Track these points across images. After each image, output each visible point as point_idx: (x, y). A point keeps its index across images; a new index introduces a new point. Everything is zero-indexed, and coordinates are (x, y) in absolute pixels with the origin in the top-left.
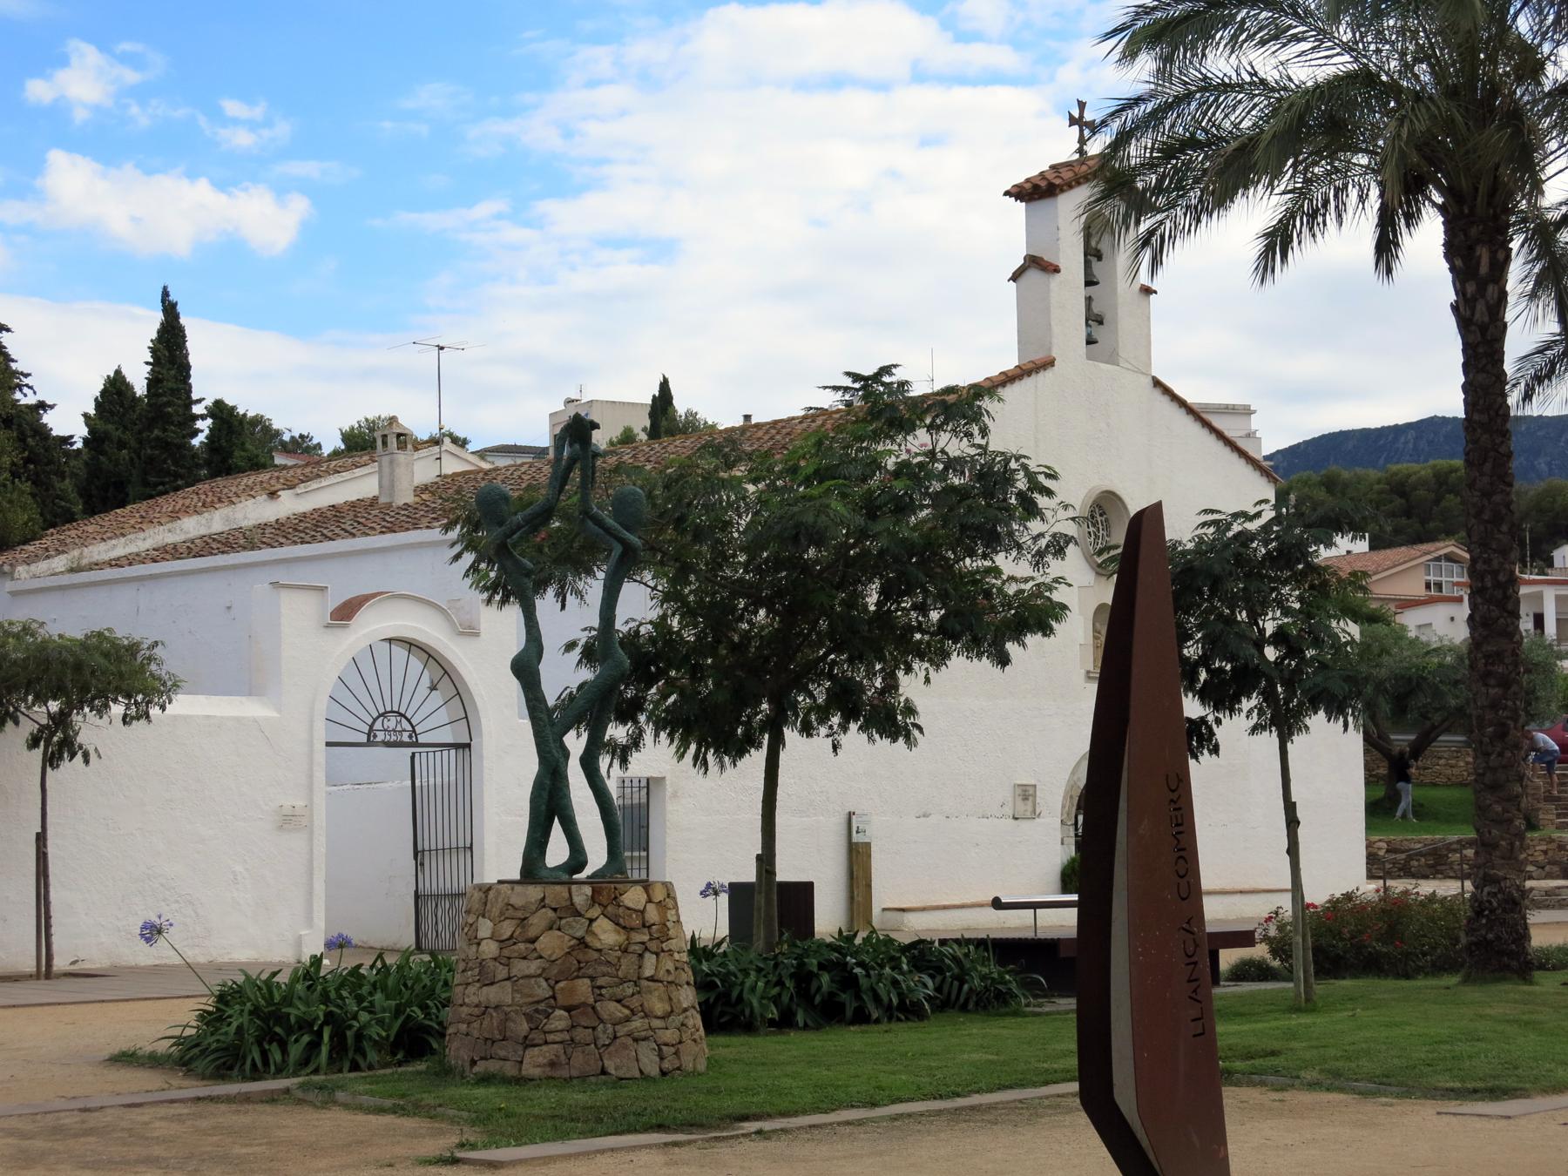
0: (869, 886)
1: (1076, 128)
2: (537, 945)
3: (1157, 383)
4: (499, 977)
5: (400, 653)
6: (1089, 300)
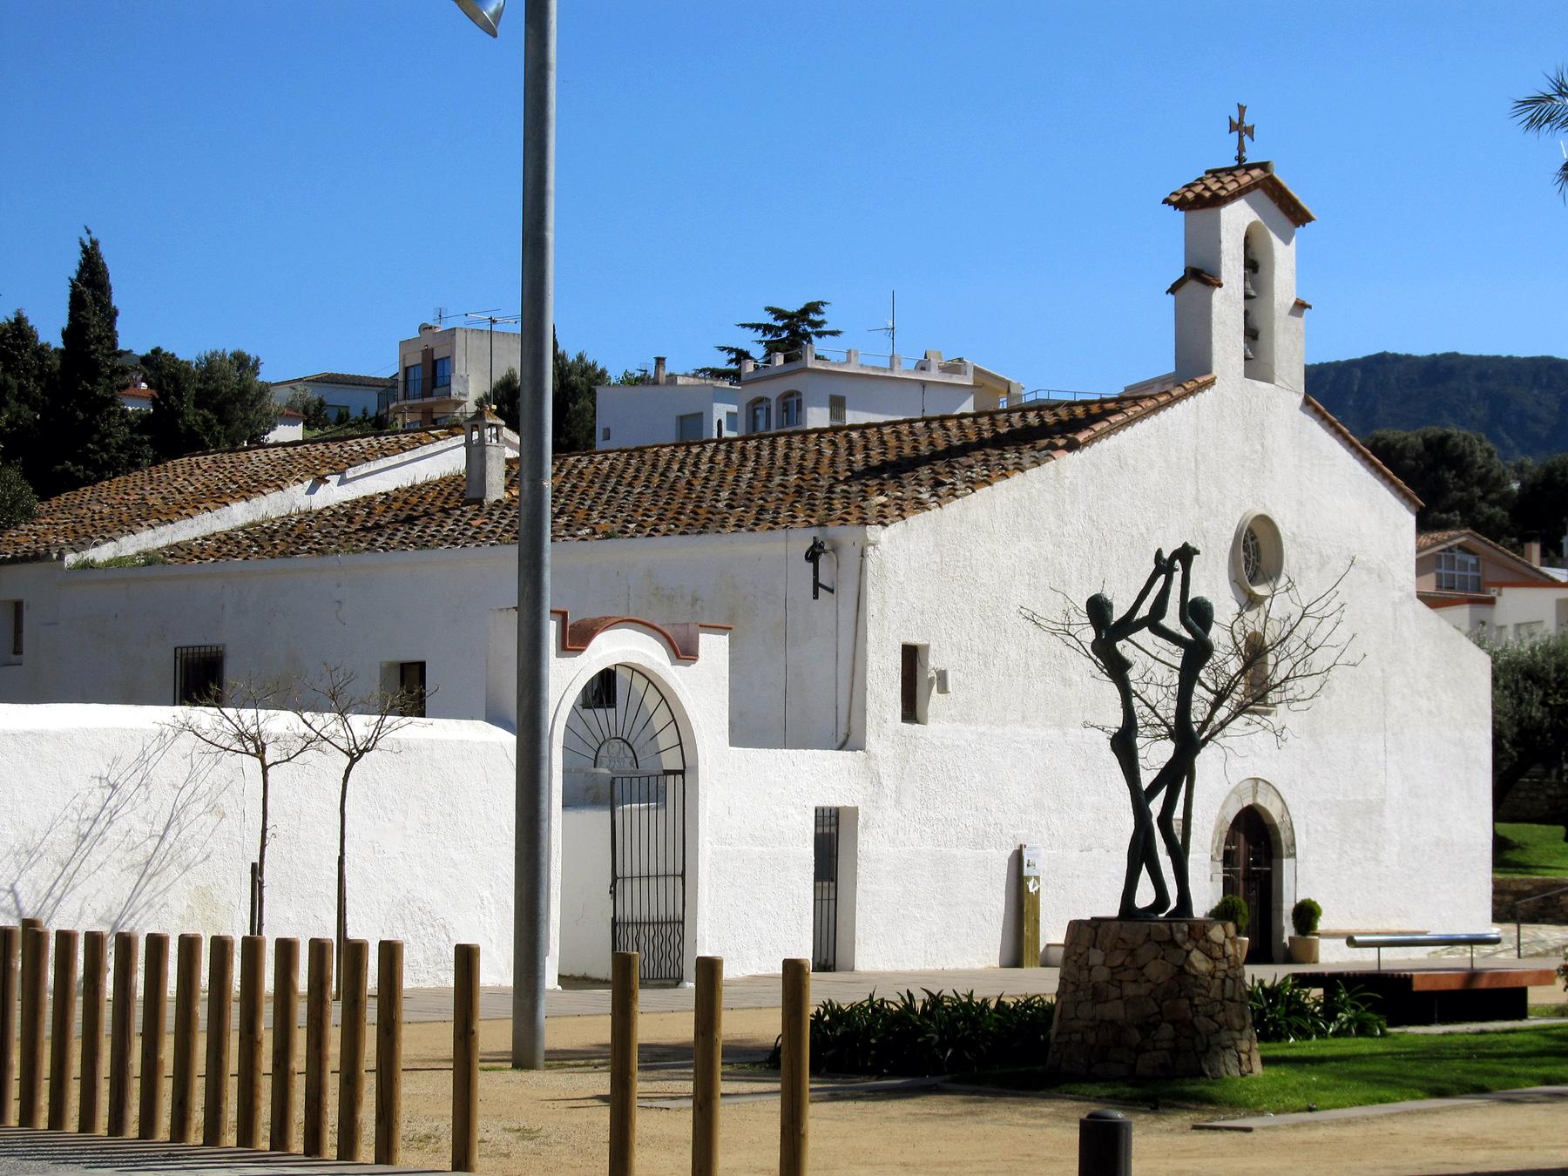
0: (1037, 921)
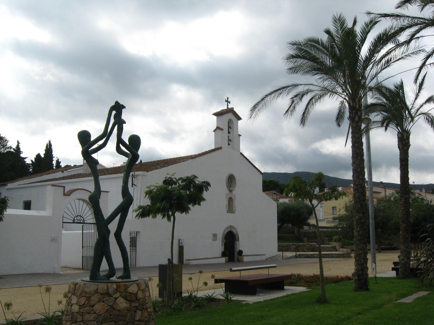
1: (229, 101)
2: (94, 308)
3: (241, 154)
4: (79, 320)
5: (81, 202)
6: (229, 136)
